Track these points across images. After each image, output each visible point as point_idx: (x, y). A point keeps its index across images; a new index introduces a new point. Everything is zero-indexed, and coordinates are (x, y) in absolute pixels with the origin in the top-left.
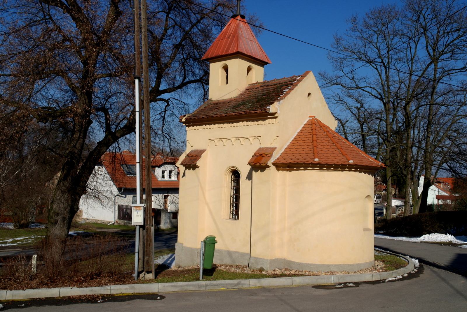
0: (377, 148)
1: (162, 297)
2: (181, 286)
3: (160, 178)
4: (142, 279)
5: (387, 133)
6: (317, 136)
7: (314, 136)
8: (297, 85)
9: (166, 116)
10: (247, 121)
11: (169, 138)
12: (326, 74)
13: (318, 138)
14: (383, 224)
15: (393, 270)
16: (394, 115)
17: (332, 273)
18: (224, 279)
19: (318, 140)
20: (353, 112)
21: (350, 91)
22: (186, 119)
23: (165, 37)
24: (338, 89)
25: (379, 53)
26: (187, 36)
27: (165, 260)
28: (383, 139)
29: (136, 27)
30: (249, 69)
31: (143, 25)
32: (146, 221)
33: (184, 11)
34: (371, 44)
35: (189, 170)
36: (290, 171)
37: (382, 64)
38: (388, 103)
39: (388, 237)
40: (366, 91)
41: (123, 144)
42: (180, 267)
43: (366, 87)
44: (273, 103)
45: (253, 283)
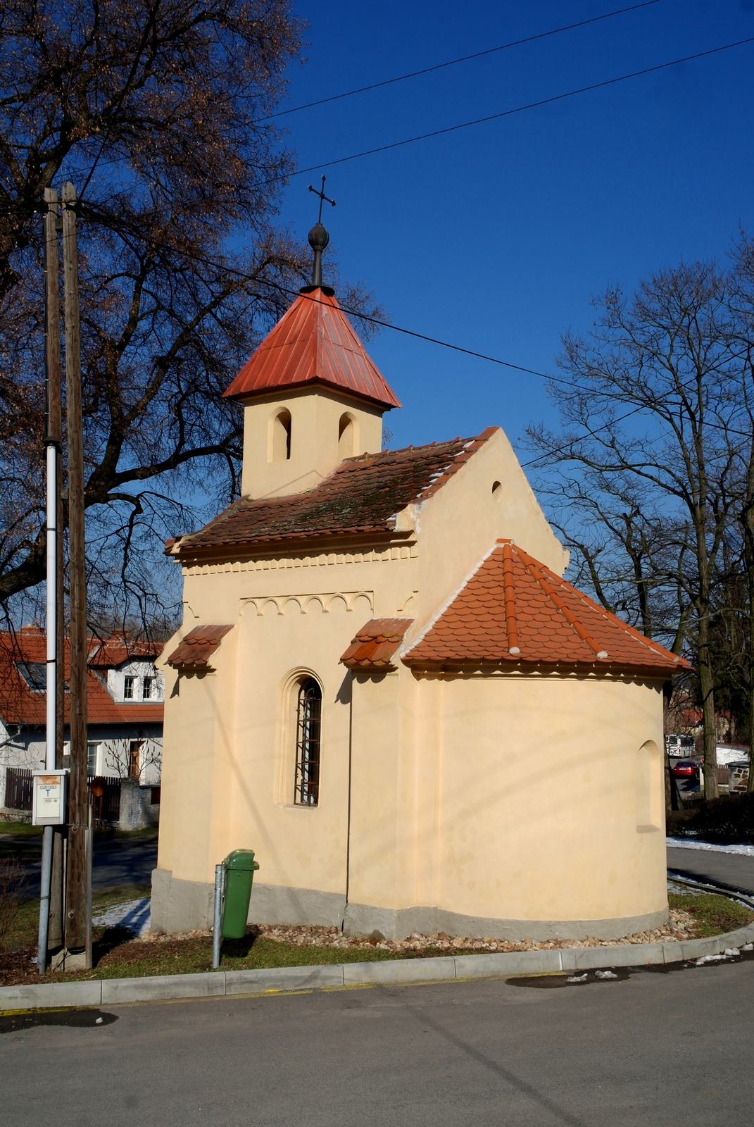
0: (677, 617)
1: (109, 1018)
2: (161, 986)
3: (119, 697)
4: (58, 969)
5: (700, 579)
6: (517, 590)
7: (510, 590)
8: (464, 462)
9: (132, 539)
10: (338, 552)
11: (140, 593)
12: (544, 434)
13: (519, 596)
14: (694, 811)
15: (716, 934)
16: (718, 534)
17: (558, 943)
18: (277, 964)
19: (517, 601)
20: (616, 527)
21: (607, 474)
22: (182, 547)
23: (132, 338)
24: (574, 470)
25: (676, 382)
26: (189, 336)
27: (125, 915)
28: (692, 596)
29: (50, 315)
30: (344, 422)
31: (67, 310)
32: (70, 814)
33: (179, 275)
34: (656, 359)
35: (189, 677)
36: (449, 678)
37: (684, 408)
38: (702, 504)
39: (708, 847)
40: (646, 476)
41: (18, 610)
42: (163, 934)
43: (645, 464)
44: (403, 507)
45: (351, 974)
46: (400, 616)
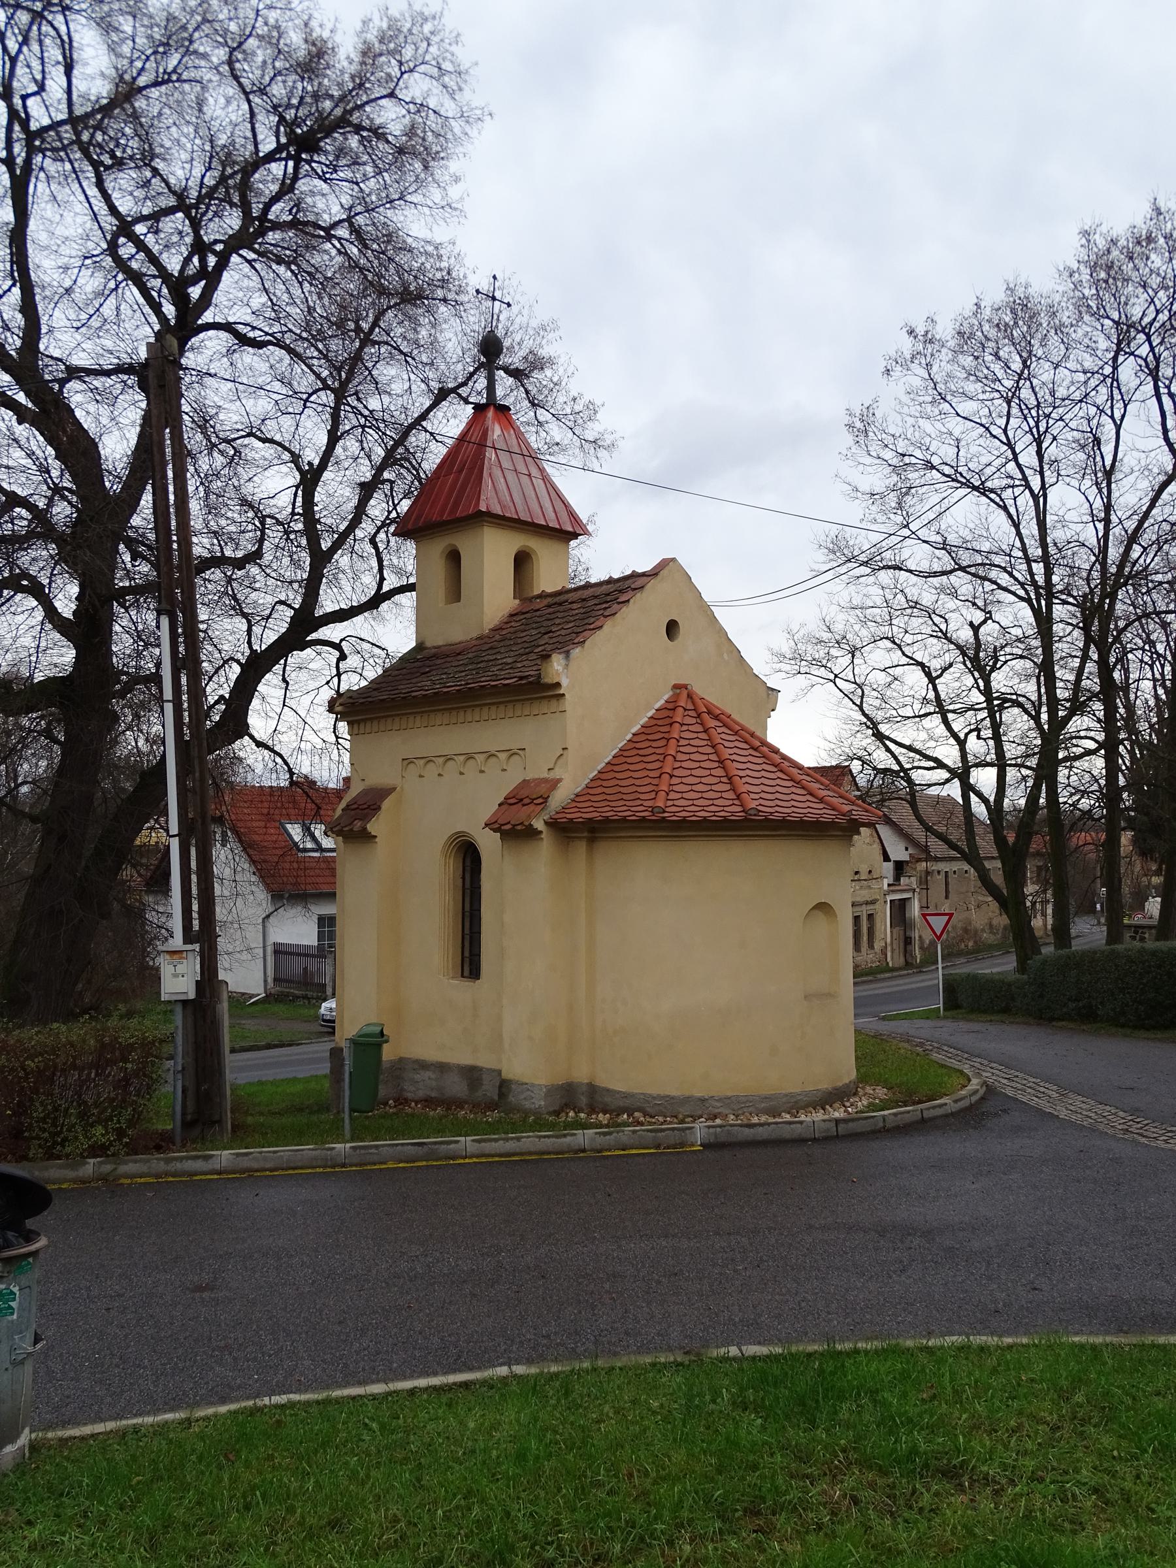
46: (552, 775)
